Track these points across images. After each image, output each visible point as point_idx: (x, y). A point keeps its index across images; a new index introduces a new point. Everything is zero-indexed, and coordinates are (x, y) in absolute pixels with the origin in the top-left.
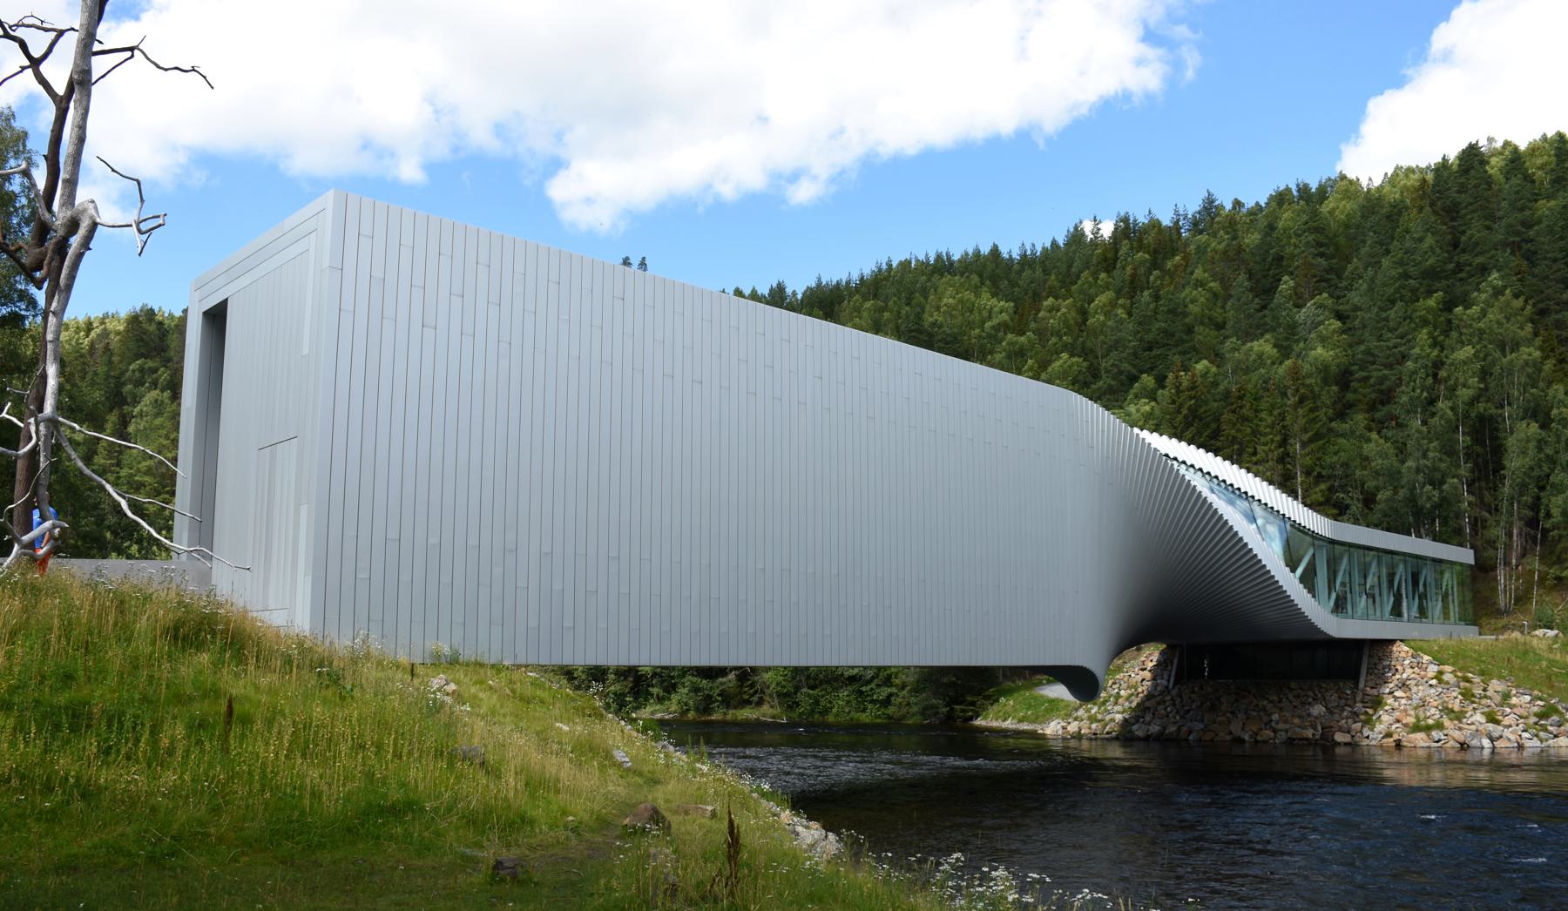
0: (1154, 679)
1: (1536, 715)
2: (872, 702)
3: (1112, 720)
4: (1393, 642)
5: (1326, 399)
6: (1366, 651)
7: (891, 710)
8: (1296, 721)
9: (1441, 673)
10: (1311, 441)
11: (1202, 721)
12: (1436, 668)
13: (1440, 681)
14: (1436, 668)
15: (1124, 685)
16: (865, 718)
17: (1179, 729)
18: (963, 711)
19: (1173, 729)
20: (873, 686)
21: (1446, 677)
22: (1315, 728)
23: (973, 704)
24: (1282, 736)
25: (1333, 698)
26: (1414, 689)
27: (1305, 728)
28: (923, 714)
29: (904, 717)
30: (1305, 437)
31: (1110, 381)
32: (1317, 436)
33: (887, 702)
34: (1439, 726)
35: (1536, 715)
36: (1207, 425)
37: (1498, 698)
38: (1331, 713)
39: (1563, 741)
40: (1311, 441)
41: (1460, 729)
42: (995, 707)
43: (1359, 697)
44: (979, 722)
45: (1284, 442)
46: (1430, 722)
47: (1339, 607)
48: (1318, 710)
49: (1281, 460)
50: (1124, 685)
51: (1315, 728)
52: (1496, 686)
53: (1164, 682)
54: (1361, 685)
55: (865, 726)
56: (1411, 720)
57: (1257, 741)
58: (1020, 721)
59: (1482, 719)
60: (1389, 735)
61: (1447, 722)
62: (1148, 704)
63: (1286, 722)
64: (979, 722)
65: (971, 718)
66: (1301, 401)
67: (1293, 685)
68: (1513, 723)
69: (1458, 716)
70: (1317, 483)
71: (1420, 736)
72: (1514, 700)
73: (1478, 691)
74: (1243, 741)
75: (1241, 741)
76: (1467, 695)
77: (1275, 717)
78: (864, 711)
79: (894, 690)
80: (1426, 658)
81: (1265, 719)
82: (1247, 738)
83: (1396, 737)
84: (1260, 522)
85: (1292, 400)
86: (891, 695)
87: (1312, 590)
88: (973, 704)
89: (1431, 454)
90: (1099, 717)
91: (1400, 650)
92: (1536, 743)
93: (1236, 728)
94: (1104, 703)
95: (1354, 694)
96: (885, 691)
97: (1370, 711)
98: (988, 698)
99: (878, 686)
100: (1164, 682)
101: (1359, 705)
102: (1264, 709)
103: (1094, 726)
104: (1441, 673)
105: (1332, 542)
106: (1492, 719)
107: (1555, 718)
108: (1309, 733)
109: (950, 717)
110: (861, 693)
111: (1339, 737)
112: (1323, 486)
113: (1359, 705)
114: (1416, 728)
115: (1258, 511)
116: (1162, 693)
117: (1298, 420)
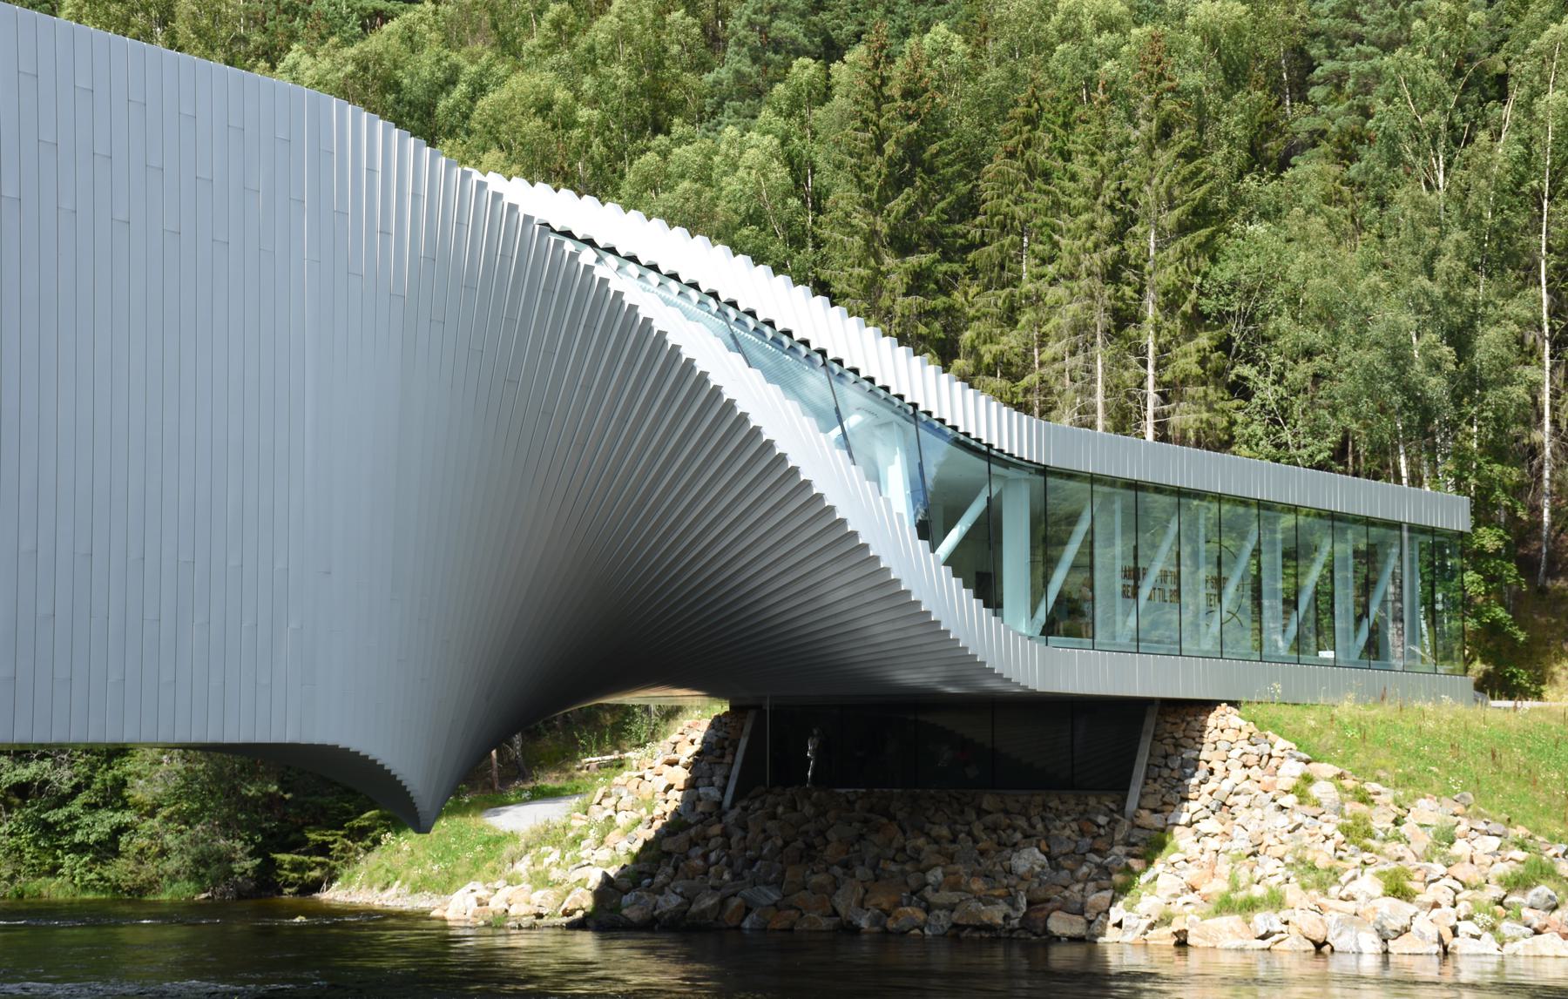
0: (691, 785)
1: (1502, 881)
2: (80, 848)
3: (582, 882)
4: (1209, 705)
5: (1233, 123)
6: (1150, 724)
7: (119, 870)
8: (978, 885)
9: (1308, 779)
10: (1183, 229)
11: (778, 883)
12: (1298, 769)
13: (1303, 798)
14: (1298, 769)
15: (627, 801)
16: (55, 890)
17: (723, 902)
18: (297, 867)
19: (708, 902)
20: (76, 806)
21: (1319, 790)
22: (1013, 904)
23: (323, 849)
24: (942, 920)
25: (1066, 831)
26: (1242, 815)
27: (989, 901)
28: (195, 877)
29: (152, 885)
30: (1170, 219)
31: (747, 67)
32: (1202, 215)
33: (108, 849)
34: (1276, 902)
35: (1502, 881)
36: (947, 185)
37: (1423, 841)
38: (1057, 868)
39: (1549, 943)
40: (1183, 229)
41: (1320, 910)
42: (373, 857)
43: (1124, 827)
44: (334, 895)
45: (1119, 234)
46: (1258, 891)
47: (1067, 619)
48: (1029, 859)
49: (1112, 275)
50: (627, 801)
51: (1013, 904)
52: (1428, 811)
53: (714, 793)
54: (1131, 805)
55: (51, 911)
56: (1219, 886)
57: (886, 931)
58: (416, 890)
59: (1377, 888)
60: (1165, 920)
61: (1292, 893)
62: (668, 845)
63: (955, 887)
64: (334, 895)
65: (317, 886)
66: (1165, 132)
67: (988, 801)
68: (1446, 898)
69: (1323, 879)
70: (1190, 333)
71: (1232, 921)
72: (1460, 848)
73: (1380, 821)
74: (857, 930)
75: (853, 930)
76: (1358, 833)
77: (935, 876)
78: (54, 871)
79: (128, 817)
80: (1281, 743)
81: (913, 882)
82: (864, 923)
83: (1177, 925)
84: (853, 421)
85: (1147, 128)
86: (119, 830)
87: (987, 588)
88: (323, 849)
89: (1442, 265)
90: (555, 874)
91: (1222, 723)
92: (1488, 944)
93: (845, 902)
94: (576, 842)
95: (1113, 823)
96: (107, 820)
97: (1136, 864)
98: (360, 834)
99: (91, 807)
100: (714, 793)
101: (1119, 850)
102: (915, 858)
103: (537, 897)
104: (1308, 779)
105: (1044, 471)
106: (1399, 891)
107: (1544, 890)
108: (995, 914)
109: (266, 881)
110: (48, 828)
111: (1060, 924)
112: (1204, 340)
113: (1119, 850)
114: (1225, 906)
115: (851, 395)
116: (705, 819)
117: (1156, 177)
